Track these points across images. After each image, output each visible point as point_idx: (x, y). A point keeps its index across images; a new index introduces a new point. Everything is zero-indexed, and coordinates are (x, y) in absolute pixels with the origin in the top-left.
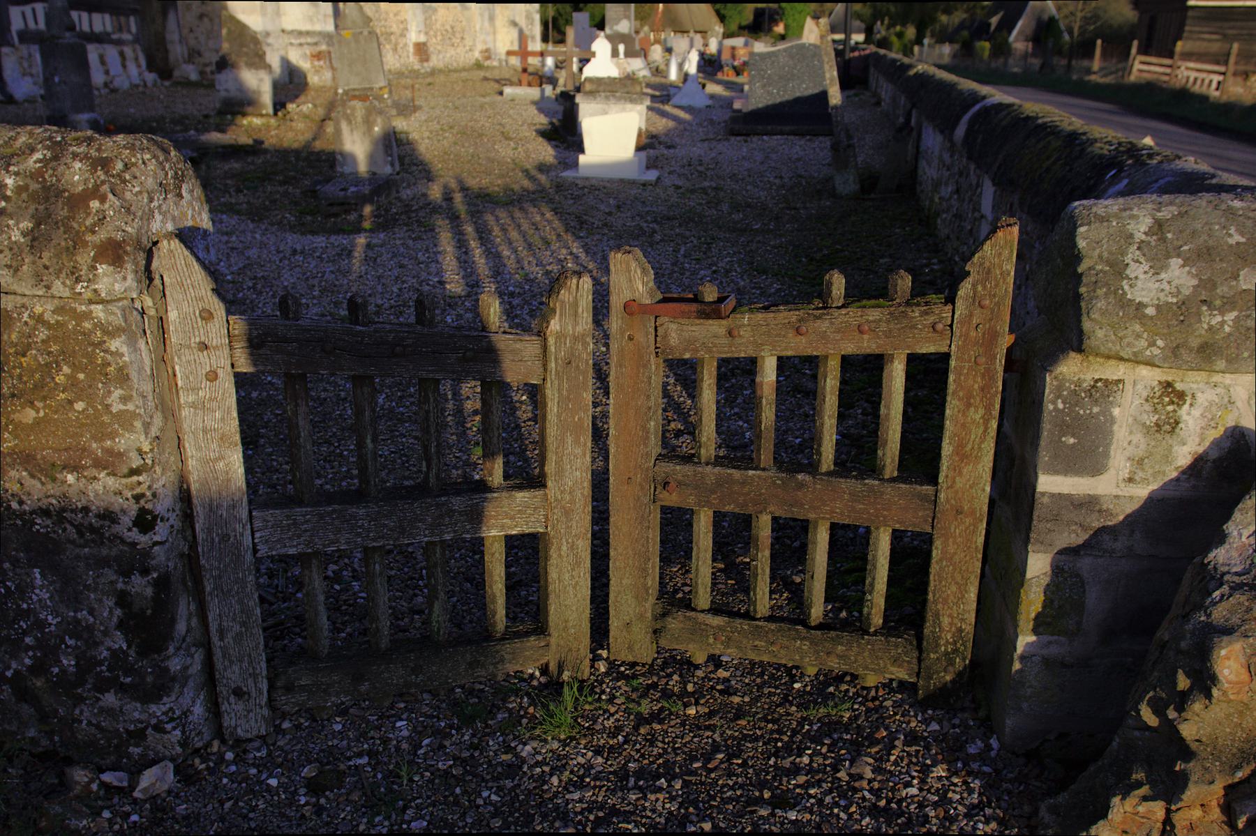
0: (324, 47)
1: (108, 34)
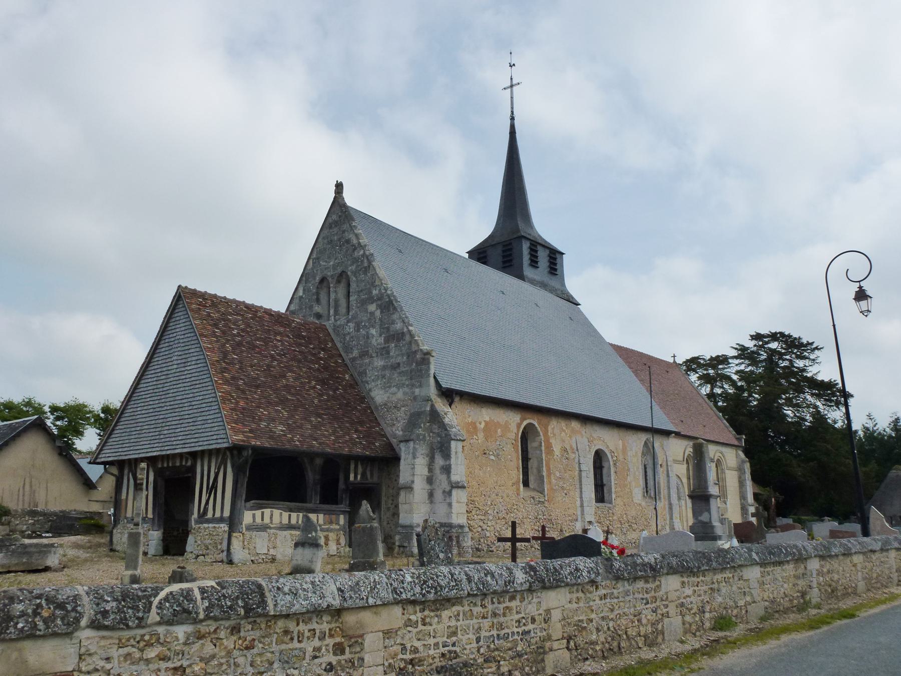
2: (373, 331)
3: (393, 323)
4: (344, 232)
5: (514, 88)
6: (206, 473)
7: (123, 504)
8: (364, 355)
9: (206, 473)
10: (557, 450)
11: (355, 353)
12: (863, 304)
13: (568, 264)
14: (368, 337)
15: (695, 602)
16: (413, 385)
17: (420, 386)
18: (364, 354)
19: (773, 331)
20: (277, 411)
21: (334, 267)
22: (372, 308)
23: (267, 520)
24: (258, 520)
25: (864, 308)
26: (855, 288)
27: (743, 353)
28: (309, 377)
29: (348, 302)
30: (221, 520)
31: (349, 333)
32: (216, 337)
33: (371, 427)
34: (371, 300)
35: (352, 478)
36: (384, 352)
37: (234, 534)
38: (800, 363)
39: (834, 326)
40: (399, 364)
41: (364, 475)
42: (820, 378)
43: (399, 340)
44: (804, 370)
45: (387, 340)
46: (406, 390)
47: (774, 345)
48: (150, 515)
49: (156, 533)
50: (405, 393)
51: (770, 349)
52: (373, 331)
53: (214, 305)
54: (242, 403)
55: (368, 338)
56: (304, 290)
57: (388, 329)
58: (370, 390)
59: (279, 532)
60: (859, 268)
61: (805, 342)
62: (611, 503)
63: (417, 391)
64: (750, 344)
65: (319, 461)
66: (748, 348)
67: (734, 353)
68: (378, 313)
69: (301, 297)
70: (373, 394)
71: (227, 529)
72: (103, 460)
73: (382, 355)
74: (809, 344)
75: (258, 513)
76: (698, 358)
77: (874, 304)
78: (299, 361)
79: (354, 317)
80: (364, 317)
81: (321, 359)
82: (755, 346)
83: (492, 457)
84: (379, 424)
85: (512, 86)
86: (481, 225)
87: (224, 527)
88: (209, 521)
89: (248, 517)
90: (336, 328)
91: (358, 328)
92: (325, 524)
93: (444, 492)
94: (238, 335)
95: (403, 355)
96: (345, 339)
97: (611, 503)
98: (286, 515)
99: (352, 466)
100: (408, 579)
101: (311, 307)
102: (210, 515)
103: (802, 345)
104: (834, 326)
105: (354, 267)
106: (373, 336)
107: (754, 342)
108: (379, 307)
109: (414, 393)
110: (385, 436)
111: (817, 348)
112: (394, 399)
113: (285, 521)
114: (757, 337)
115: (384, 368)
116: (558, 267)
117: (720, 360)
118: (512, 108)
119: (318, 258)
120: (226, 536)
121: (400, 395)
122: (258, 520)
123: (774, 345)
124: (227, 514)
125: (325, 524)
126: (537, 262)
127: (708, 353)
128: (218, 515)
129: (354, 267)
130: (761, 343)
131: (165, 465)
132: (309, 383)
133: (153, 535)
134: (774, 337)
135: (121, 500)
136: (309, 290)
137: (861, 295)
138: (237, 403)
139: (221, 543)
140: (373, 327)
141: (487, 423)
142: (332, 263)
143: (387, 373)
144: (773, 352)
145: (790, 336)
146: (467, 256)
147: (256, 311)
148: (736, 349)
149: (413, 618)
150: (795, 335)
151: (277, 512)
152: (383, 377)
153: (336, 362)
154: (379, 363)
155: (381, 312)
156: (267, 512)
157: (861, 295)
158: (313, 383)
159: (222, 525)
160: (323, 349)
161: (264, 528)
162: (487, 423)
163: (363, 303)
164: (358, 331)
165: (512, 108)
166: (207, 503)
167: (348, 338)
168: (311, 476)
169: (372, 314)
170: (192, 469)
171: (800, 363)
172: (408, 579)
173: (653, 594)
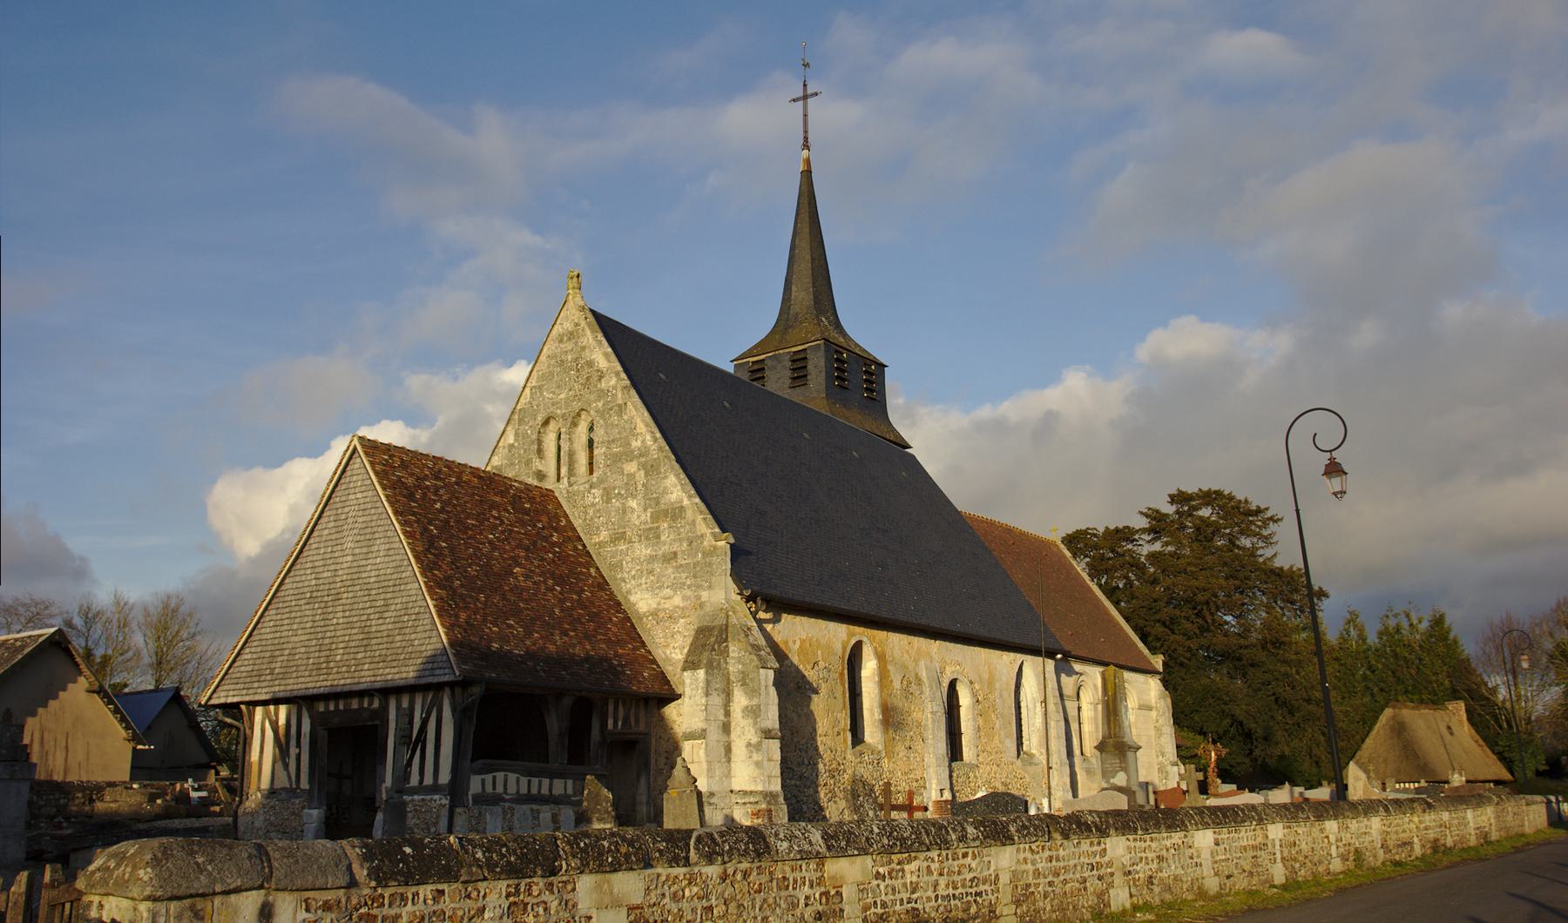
0: (764, 806)
1: (569, 797)
2: (633, 503)
3: (665, 492)
4: (583, 348)
5: (809, 100)
7: (255, 768)
8: (618, 539)
11: (604, 535)
12: (1336, 483)
14: (624, 511)
15: (1142, 871)
16: (699, 587)
17: (710, 587)
18: (618, 537)
19: (1205, 489)
20: (510, 626)
22: (631, 467)
23: (500, 789)
24: (489, 789)
25: (1338, 489)
26: (1324, 459)
27: (1158, 524)
28: (543, 574)
29: (591, 457)
30: (435, 788)
31: (593, 505)
32: (414, 514)
33: (635, 649)
34: (629, 455)
35: (610, 722)
36: (651, 535)
37: (458, 810)
38: (1246, 542)
39: (1297, 511)
41: (626, 720)
42: (1277, 563)
43: (674, 518)
44: (1253, 555)
45: (656, 518)
46: (688, 593)
47: (1205, 512)
48: (305, 785)
49: (315, 812)
50: (685, 598)
51: (1201, 518)
52: (633, 503)
53: (404, 465)
54: (463, 616)
55: (624, 512)
56: (516, 435)
57: (658, 503)
58: (629, 592)
59: (517, 807)
60: (1330, 433)
63: (705, 595)
64: (1169, 509)
65: (567, 701)
66: (1167, 515)
67: (1143, 523)
69: (511, 446)
70: (633, 598)
71: (445, 801)
72: (222, 701)
73: (647, 538)
74: (1259, 511)
75: (489, 778)
76: (1085, 532)
77: (1351, 482)
78: (527, 549)
79: (601, 481)
80: (617, 481)
81: (555, 544)
84: (643, 644)
85: (805, 97)
87: (443, 800)
88: (413, 791)
89: (475, 784)
90: (571, 496)
92: (575, 794)
93: (749, 745)
94: (442, 510)
95: (681, 540)
98: (524, 780)
99: (611, 708)
100: (876, 830)
101: (528, 462)
102: (414, 781)
104: (1297, 511)
105: (600, 404)
106: (633, 510)
108: (643, 466)
109: (699, 598)
110: (654, 661)
111: (1271, 519)
112: (668, 605)
113: (524, 790)
114: (1179, 498)
115: (652, 559)
118: (806, 132)
119: (540, 388)
120: (445, 813)
121: (677, 600)
122: (489, 789)
123: (1205, 512)
124: (445, 777)
125: (575, 794)
128: (428, 780)
129: (600, 404)
132: (545, 582)
133: (310, 815)
134: (1210, 497)
135: (250, 764)
136: (525, 435)
137: (1334, 469)
138: (457, 616)
139: (436, 824)
140: (633, 496)
141: (803, 641)
143: (657, 567)
145: (1231, 498)
147: (462, 473)
148: (1147, 516)
149: (881, 870)
150: (1240, 496)
151: (512, 777)
152: (651, 572)
153: (575, 549)
154: (643, 550)
155: (646, 474)
156: (500, 775)
157: (1334, 469)
158: (550, 582)
159: (436, 797)
160: (555, 529)
161: (495, 800)
162: (803, 641)
163: (616, 460)
164: (608, 501)
165: (806, 132)
167: (591, 512)
168: (554, 724)
169: (631, 476)
171: (1246, 542)
172: (876, 830)
173: (1098, 859)
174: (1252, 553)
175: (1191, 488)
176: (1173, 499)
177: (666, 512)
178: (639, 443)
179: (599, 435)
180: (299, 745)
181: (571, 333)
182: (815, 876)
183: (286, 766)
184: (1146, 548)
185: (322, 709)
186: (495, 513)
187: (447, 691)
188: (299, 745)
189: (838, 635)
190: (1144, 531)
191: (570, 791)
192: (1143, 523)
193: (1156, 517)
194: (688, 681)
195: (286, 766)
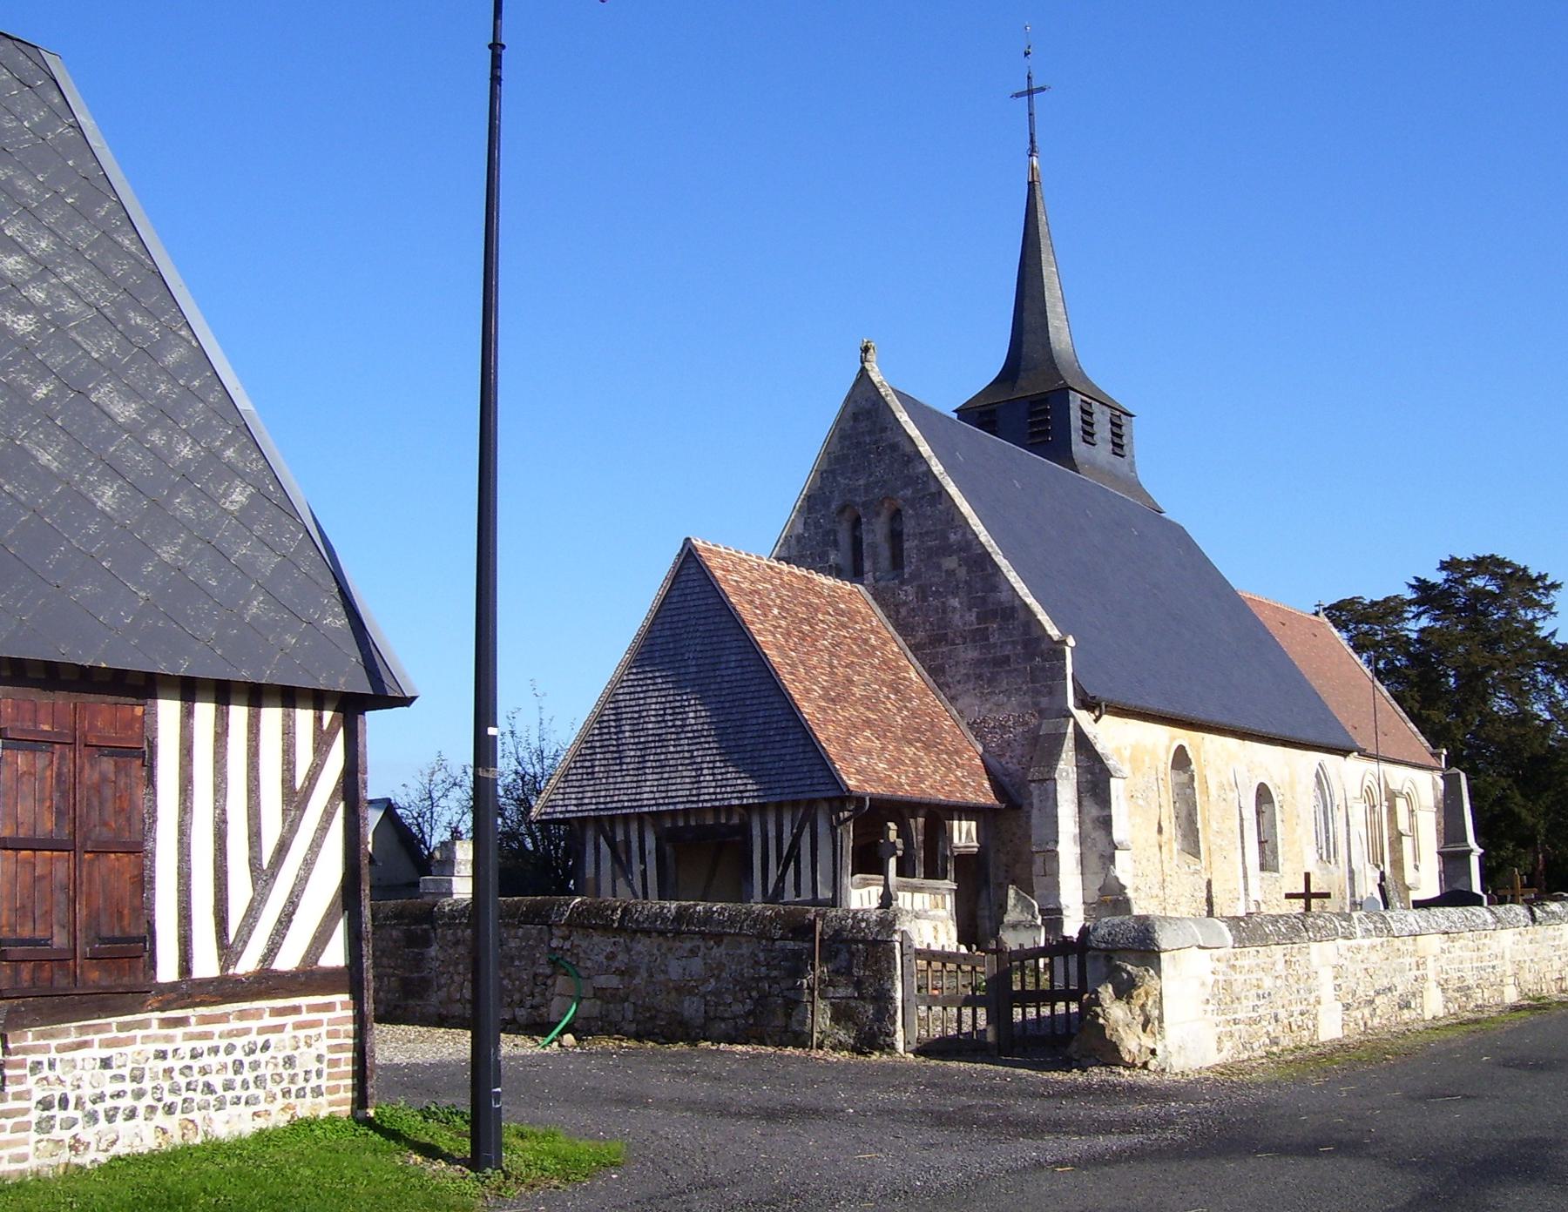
6: (772, 833)
9: (772, 833)
10: (1213, 790)
13: (1139, 434)
21: (868, 488)
22: (950, 563)
27: (1426, 593)
31: (905, 603)
34: (947, 550)
40: (1008, 657)
47: (1479, 582)
52: (955, 602)
55: (944, 612)
57: (984, 600)
61: (1535, 575)
62: (1276, 870)
64: (1438, 577)
66: (1434, 586)
68: (962, 573)
74: (1542, 577)
79: (915, 576)
82: (1446, 581)
83: (1140, 802)
85: (1030, 92)
86: (976, 365)
91: (923, 593)
93: (1102, 856)
96: (898, 612)
97: (1276, 870)
103: (1532, 581)
107: (1444, 574)
108: (964, 562)
114: (1449, 565)
115: (978, 663)
116: (1125, 440)
117: (1390, 609)
123: (1479, 582)
126: (1092, 435)
127: (1373, 592)
129: (909, 492)
130: (1457, 576)
131: (681, 824)
134: (1483, 565)
140: (955, 595)
142: (861, 482)
144: (1479, 593)
146: (955, 416)
164: (925, 599)
166: (781, 879)
167: (903, 611)
169: (951, 573)
170: (745, 830)
174: (1530, 626)
175: (1465, 554)
176: (1444, 566)
177: (994, 614)
178: (959, 536)
179: (909, 526)
180: (643, 860)
181: (869, 412)
182: (1411, 948)
183: (630, 884)
184: (1414, 625)
185: (668, 825)
186: (820, 616)
187: (826, 806)
188: (643, 860)
189: (1160, 739)
190: (1411, 603)
191: (927, 906)
192: (1410, 595)
193: (1422, 586)
194: (1036, 793)
195: (630, 884)
